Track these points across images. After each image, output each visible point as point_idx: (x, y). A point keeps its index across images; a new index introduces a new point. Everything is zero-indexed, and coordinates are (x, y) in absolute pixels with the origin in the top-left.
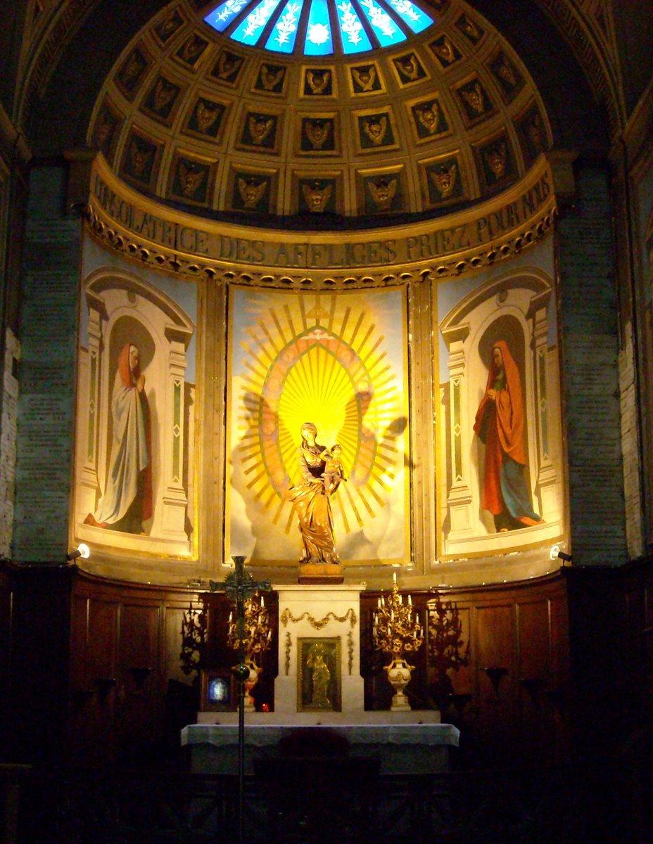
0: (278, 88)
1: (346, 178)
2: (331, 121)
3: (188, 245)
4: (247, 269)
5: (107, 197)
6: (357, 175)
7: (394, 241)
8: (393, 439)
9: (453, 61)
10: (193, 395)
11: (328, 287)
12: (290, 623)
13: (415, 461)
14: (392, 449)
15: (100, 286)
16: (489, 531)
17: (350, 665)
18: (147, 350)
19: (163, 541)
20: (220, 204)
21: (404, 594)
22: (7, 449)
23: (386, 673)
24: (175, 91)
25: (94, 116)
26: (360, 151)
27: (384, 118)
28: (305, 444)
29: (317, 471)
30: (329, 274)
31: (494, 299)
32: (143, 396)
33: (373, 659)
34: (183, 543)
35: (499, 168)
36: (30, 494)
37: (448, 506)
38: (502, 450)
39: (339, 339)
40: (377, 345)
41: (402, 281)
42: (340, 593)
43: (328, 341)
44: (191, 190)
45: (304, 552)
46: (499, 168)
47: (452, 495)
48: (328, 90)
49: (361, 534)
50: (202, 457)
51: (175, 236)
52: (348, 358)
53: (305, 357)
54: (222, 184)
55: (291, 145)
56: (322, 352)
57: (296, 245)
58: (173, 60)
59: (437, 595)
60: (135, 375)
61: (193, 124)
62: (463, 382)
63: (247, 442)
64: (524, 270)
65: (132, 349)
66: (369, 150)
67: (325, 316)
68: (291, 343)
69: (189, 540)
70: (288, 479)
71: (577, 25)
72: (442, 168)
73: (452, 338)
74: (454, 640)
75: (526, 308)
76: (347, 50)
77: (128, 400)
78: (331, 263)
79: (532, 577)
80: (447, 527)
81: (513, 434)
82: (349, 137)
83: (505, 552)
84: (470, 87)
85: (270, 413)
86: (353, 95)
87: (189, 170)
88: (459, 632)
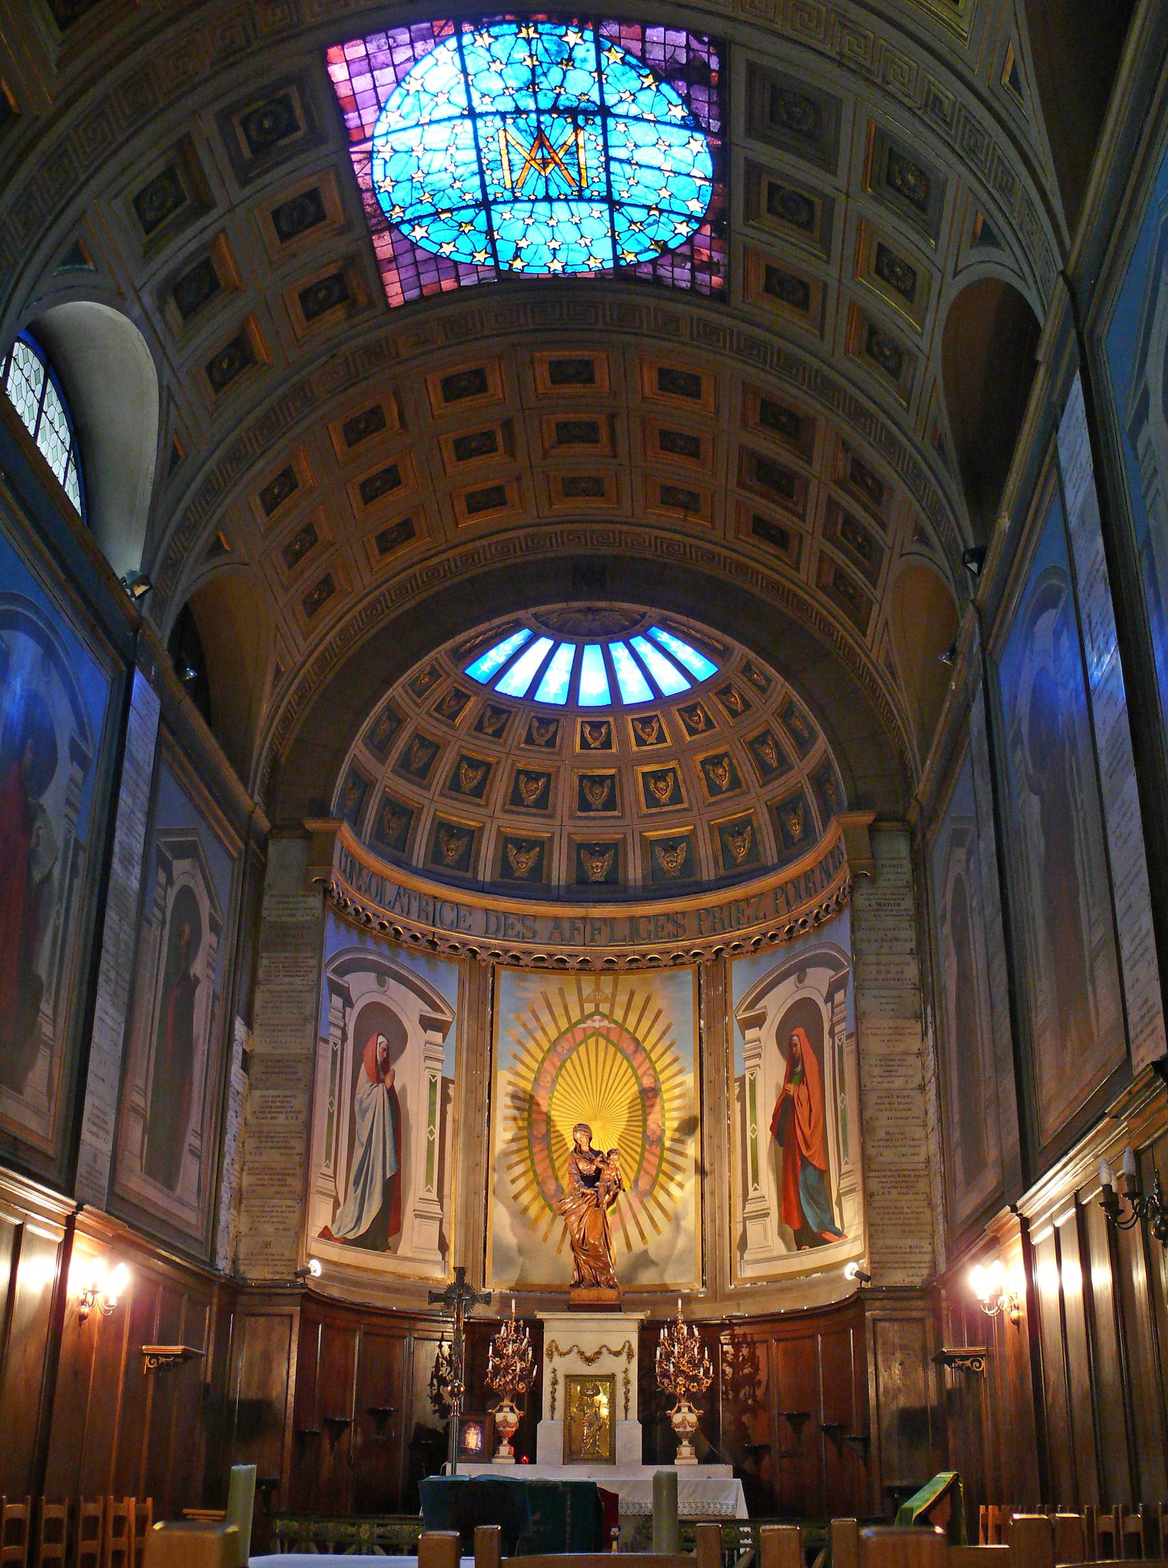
0: (551, 743)
1: (630, 841)
2: (612, 777)
3: (447, 921)
4: (516, 947)
5: (354, 869)
6: (643, 839)
7: (683, 913)
8: (682, 1142)
9: (743, 711)
10: (451, 1092)
11: (609, 967)
12: (556, 1357)
13: (707, 1167)
14: (682, 1154)
15: (342, 971)
16: (789, 1249)
17: (626, 1409)
18: (399, 1040)
19: (413, 1260)
20: (486, 872)
22: (232, 1151)
23: (669, 1419)
24: (434, 748)
25: (340, 783)
26: (645, 811)
27: (671, 774)
28: (578, 1149)
29: (590, 1181)
30: (610, 952)
31: (792, 979)
32: (391, 1092)
33: (654, 1404)
34: (437, 1263)
35: (797, 830)
36: (258, 1202)
37: (745, 1220)
38: (802, 1155)
39: (622, 1027)
40: (664, 1033)
41: (692, 960)
42: (614, 1323)
43: (609, 1029)
44: (453, 857)
45: (576, 1274)
46: (797, 830)
47: (749, 1208)
48: (607, 744)
49: (645, 1253)
50: (460, 1164)
51: (432, 909)
52: (632, 1047)
53: (582, 1049)
54: (488, 850)
55: (566, 805)
56: (602, 1042)
57: (572, 919)
58: (431, 716)
59: (731, 1326)
60: (383, 1069)
61: (454, 785)
62: (760, 1074)
63: (514, 1146)
64: (823, 945)
65: (381, 1039)
66: (654, 810)
67: (606, 1000)
68: (565, 1033)
69: (443, 1259)
71: (869, 673)
72: (737, 828)
73: (748, 1024)
74: (751, 1380)
75: (825, 989)
76: (627, 699)
78: (613, 939)
80: (743, 1244)
81: (812, 1135)
82: (634, 790)
83: (808, 1273)
84: (762, 739)
85: (541, 1113)
86: (635, 749)
87: (452, 836)
88: (756, 1368)
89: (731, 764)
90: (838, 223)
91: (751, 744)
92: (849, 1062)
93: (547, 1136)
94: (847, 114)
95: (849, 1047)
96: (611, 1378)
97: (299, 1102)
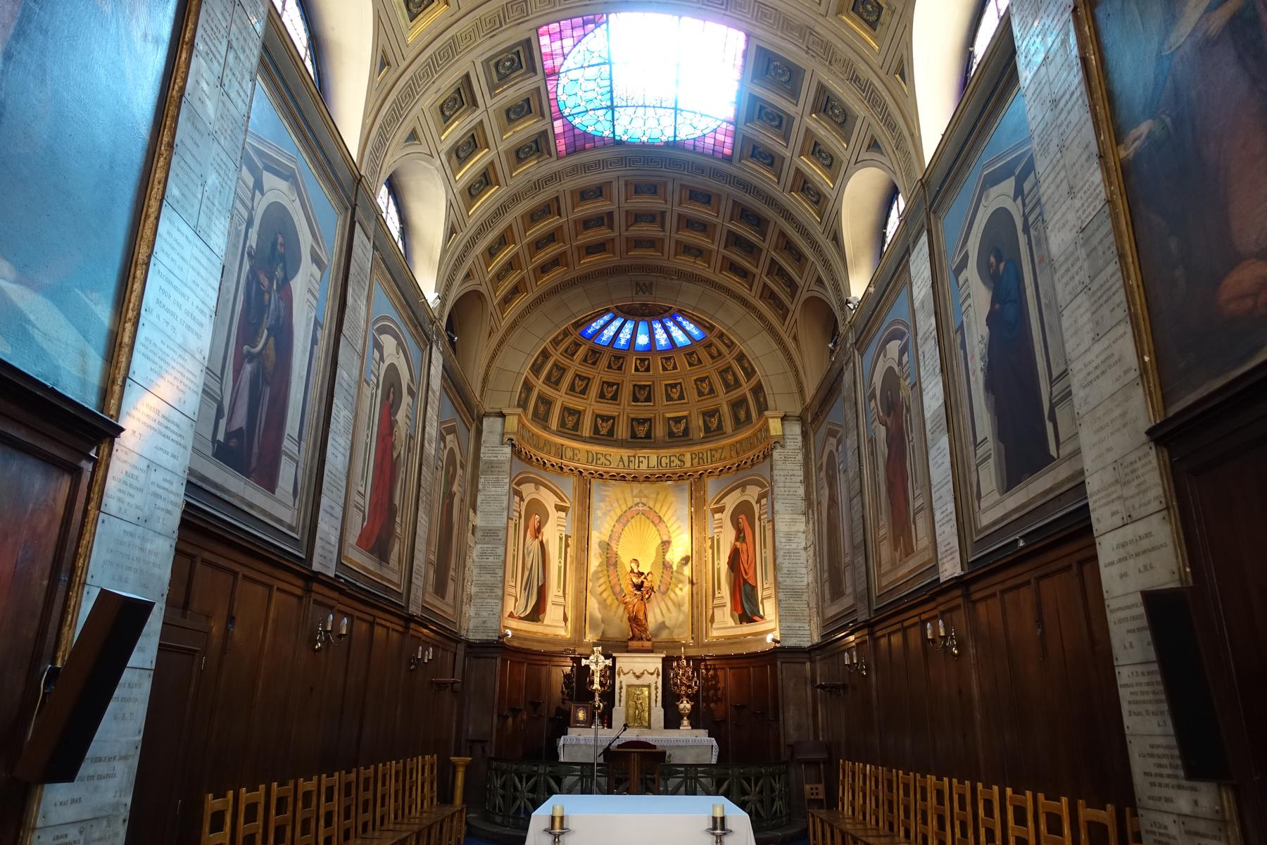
0: (620, 368)
10: (570, 541)
15: (519, 484)
18: (545, 517)
21: (688, 659)
24: (562, 370)
28: (632, 571)
29: (639, 587)
32: (542, 543)
33: (670, 698)
46: (742, 415)
48: (648, 370)
60: (538, 530)
62: (722, 536)
70: (622, 590)
77: (534, 545)
79: (45, 583)
80: (712, 620)
82: (660, 393)
83: (745, 636)
88: (718, 682)
89: (710, 384)
90: (795, 129)
91: (720, 373)
92: (769, 534)
93: (615, 564)
94: (807, 76)
95: (769, 526)
96: (649, 686)
97: (500, 551)
